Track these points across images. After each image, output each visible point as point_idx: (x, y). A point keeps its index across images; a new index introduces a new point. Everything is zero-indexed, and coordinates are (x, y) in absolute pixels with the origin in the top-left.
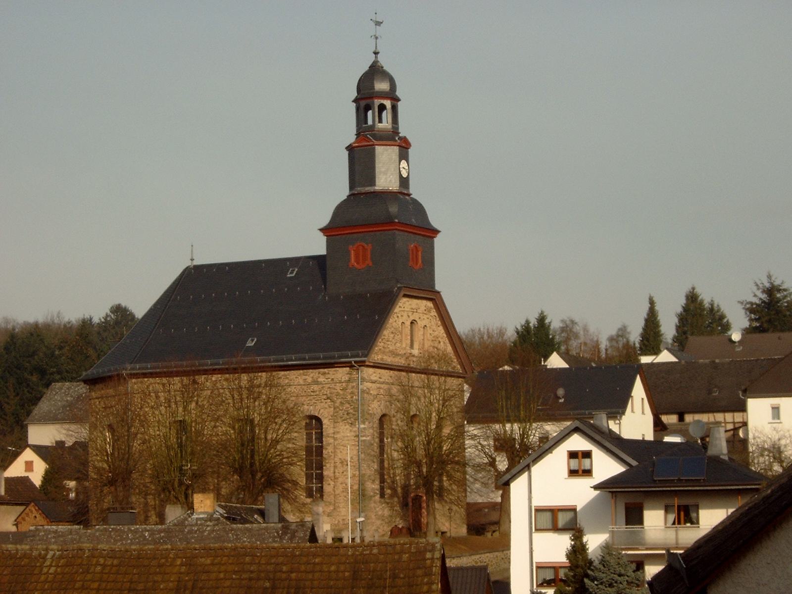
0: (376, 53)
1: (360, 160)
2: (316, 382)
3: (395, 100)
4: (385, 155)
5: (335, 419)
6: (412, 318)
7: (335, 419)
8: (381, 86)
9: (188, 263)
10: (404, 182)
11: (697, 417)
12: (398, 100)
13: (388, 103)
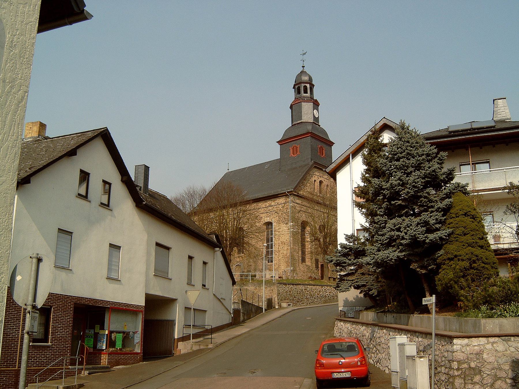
0: (303, 67)
1: (295, 108)
2: (271, 206)
3: (312, 86)
4: (307, 107)
5: (279, 222)
6: (320, 179)
7: (279, 222)
8: (305, 78)
9: (227, 171)
10: (316, 119)
11: (118, 367)
12: (314, 86)
13: (308, 86)
